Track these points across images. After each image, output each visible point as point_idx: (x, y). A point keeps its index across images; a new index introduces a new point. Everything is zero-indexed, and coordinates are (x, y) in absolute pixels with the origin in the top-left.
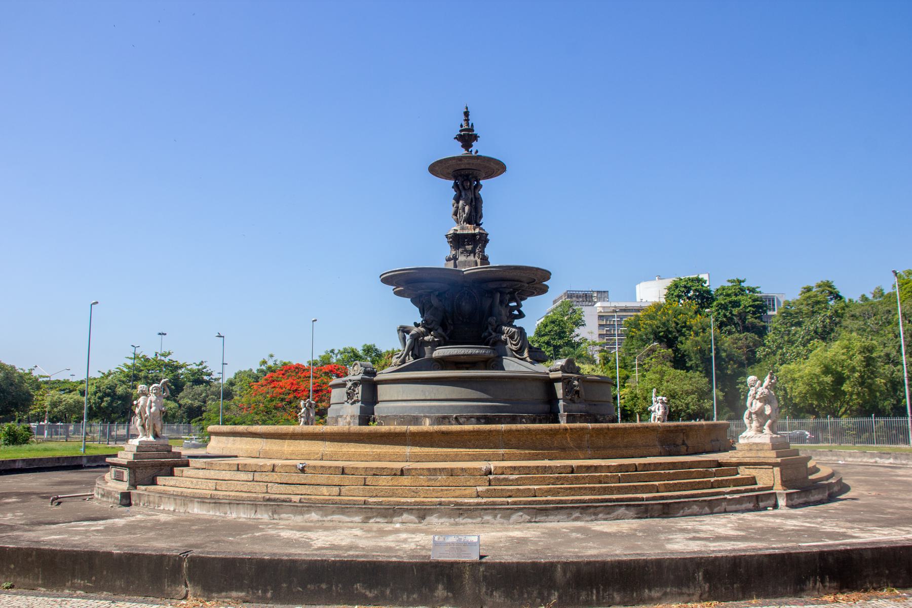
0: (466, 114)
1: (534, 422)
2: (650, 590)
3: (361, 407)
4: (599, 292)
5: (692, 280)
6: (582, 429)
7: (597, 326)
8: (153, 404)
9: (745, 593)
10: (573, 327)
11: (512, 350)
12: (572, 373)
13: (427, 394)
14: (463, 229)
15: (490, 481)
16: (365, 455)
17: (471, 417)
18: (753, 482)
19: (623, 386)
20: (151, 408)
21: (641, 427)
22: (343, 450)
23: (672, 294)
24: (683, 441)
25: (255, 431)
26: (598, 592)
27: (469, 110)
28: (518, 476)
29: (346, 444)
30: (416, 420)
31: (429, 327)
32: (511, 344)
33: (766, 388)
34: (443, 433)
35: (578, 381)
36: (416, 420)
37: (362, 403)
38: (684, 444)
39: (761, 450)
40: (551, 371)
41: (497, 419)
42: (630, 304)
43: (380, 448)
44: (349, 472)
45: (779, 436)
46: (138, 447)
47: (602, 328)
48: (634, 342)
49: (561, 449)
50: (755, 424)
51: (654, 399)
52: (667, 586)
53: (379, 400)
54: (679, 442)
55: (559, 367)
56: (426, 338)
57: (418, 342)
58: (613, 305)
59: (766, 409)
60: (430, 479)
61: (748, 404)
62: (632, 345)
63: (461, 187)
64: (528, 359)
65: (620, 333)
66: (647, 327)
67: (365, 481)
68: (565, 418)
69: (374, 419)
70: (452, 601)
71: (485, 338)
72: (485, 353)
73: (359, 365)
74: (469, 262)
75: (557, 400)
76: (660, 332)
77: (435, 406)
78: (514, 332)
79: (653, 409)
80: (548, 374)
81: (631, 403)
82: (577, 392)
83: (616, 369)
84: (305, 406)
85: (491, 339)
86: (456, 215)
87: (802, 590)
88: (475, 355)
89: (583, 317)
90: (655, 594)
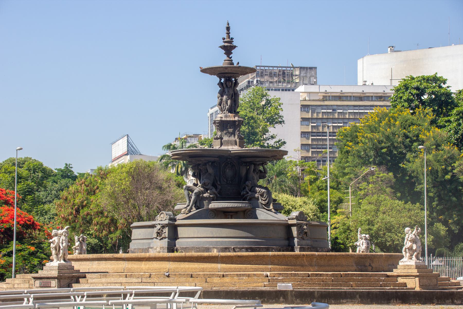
0: (228, 29)
1: (280, 251)
2: (343, 300)
3: (168, 241)
4: (304, 68)
5: (428, 80)
6: (312, 255)
7: (300, 120)
8: (64, 242)
9: (371, 302)
10: (266, 126)
11: (262, 204)
12: (302, 221)
13: (214, 233)
14: (226, 117)
15: (269, 280)
16: (195, 269)
17: (242, 248)
18: (405, 285)
19: (335, 213)
20: (62, 244)
21: (345, 255)
22: (181, 266)
23: (401, 98)
24: (370, 264)
25: (120, 257)
26: (327, 300)
27: (230, 26)
28: (282, 278)
29: (182, 263)
30: (208, 250)
31: (206, 187)
32: (262, 200)
33: (414, 235)
34: (239, 257)
35: (306, 226)
36: (208, 250)
37: (168, 239)
38: (370, 265)
39: (410, 269)
40: (289, 219)
41: (258, 249)
42: (348, 89)
43: (203, 265)
44: (195, 276)
45: (421, 261)
46: (58, 267)
47: (306, 123)
48: (350, 158)
49: (301, 266)
50: (408, 254)
51: (359, 236)
52: (348, 299)
53: (179, 237)
54: (367, 264)
55: (295, 217)
56: (205, 195)
57: (199, 198)
58: (323, 89)
59: (414, 246)
60: (240, 278)
61: (405, 244)
62: (347, 162)
63: (224, 86)
64: (273, 210)
65: (331, 130)
66: (367, 141)
67: (206, 280)
68: (298, 249)
69: (177, 249)
70: (285, 302)
71: (244, 195)
72: (245, 206)
73: (165, 214)
74: (231, 141)
75: (293, 238)
76: (382, 148)
77: (219, 241)
78: (264, 192)
79: (358, 244)
80: (287, 221)
81: (343, 235)
82: (306, 233)
83: (326, 190)
84: (79, 240)
85: (248, 196)
86: (221, 105)
87: (390, 303)
88: (239, 207)
89: (280, 112)
90: (344, 301)
